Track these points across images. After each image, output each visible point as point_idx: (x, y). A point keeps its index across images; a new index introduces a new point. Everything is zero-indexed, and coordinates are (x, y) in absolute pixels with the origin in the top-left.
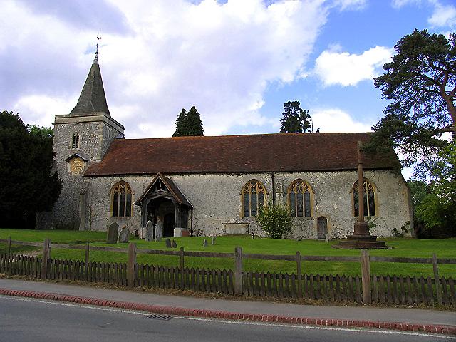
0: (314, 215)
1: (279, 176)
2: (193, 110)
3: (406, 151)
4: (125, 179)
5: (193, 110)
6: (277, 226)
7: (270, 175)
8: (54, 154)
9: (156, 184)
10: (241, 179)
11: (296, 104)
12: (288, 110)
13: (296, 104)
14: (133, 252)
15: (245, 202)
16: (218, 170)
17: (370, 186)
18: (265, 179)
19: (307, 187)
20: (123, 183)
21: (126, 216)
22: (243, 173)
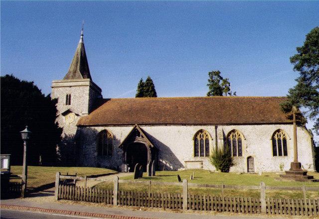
0: (245, 155)
1: (220, 128)
2: (149, 80)
3: (309, 66)
4: (107, 128)
5: (149, 80)
6: (224, 162)
7: (213, 127)
8: (57, 111)
9: (134, 134)
10: (194, 130)
11: (217, 74)
12: (212, 77)
13: (217, 74)
14: (313, 129)
15: (196, 145)
16: (176, 122)
17: (284, 135)
18: (210, 130)
19: (207, 136)
20: (105, 131)
21: (239, 156)
22: (195, 125)
